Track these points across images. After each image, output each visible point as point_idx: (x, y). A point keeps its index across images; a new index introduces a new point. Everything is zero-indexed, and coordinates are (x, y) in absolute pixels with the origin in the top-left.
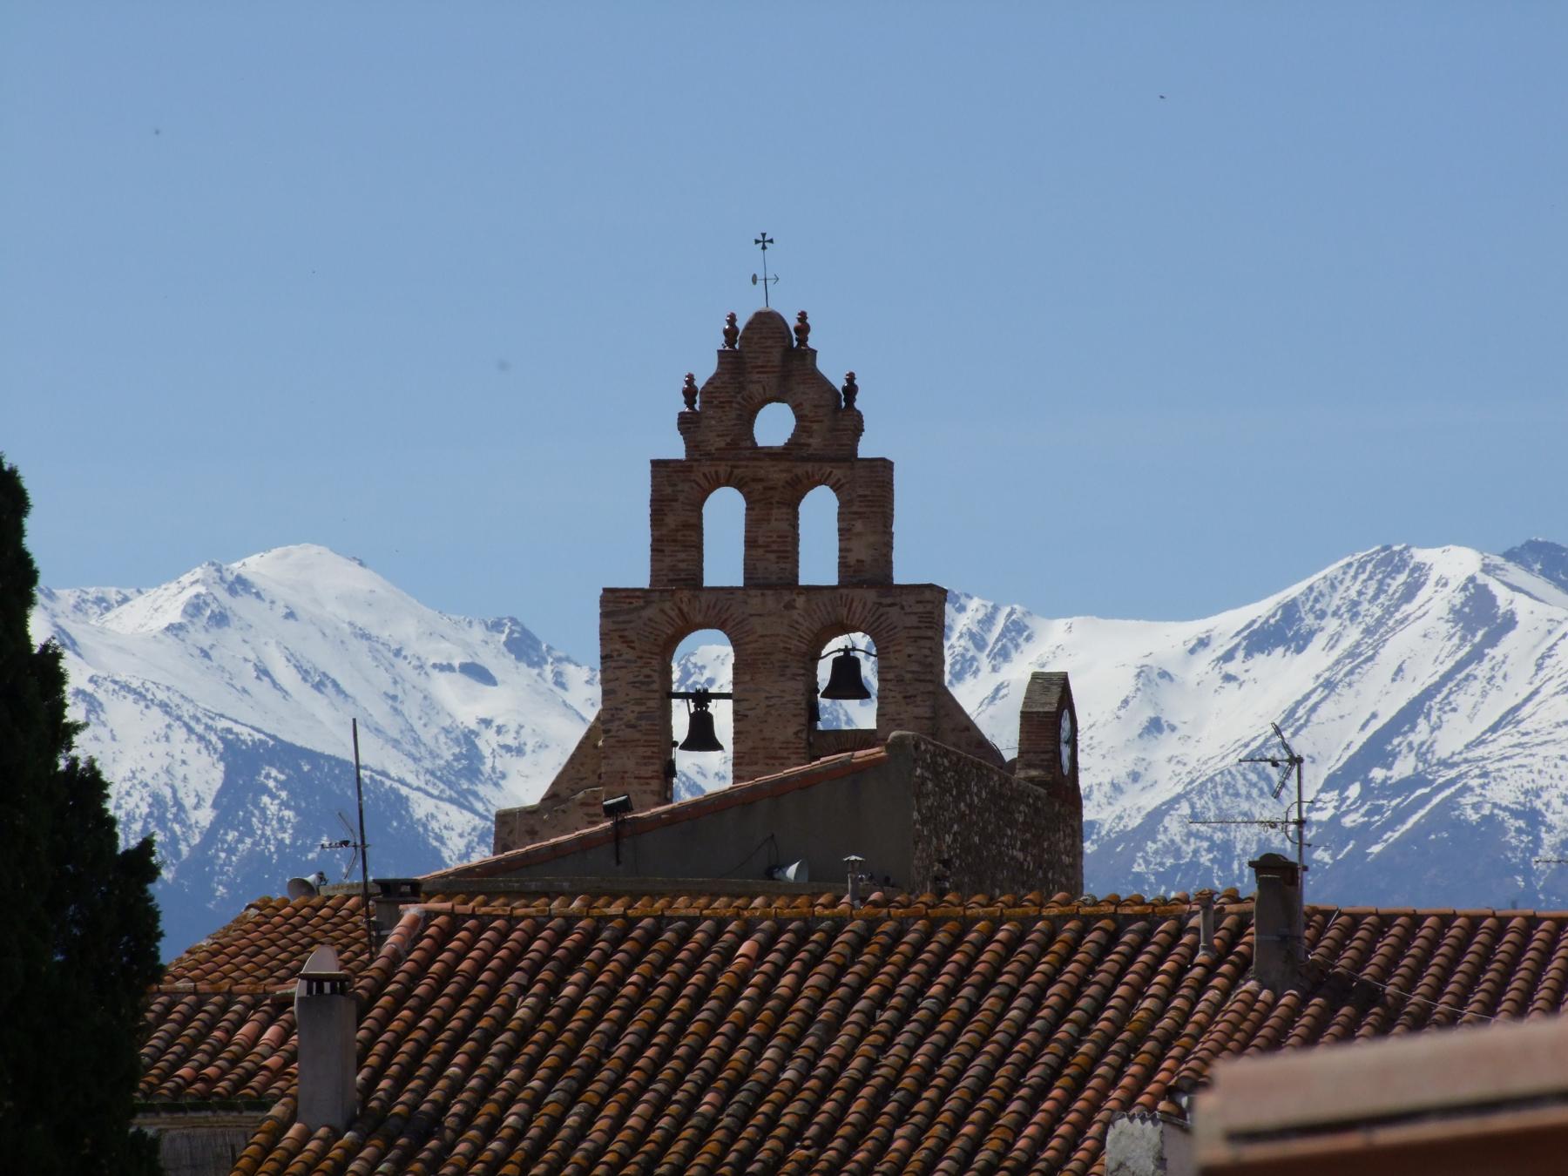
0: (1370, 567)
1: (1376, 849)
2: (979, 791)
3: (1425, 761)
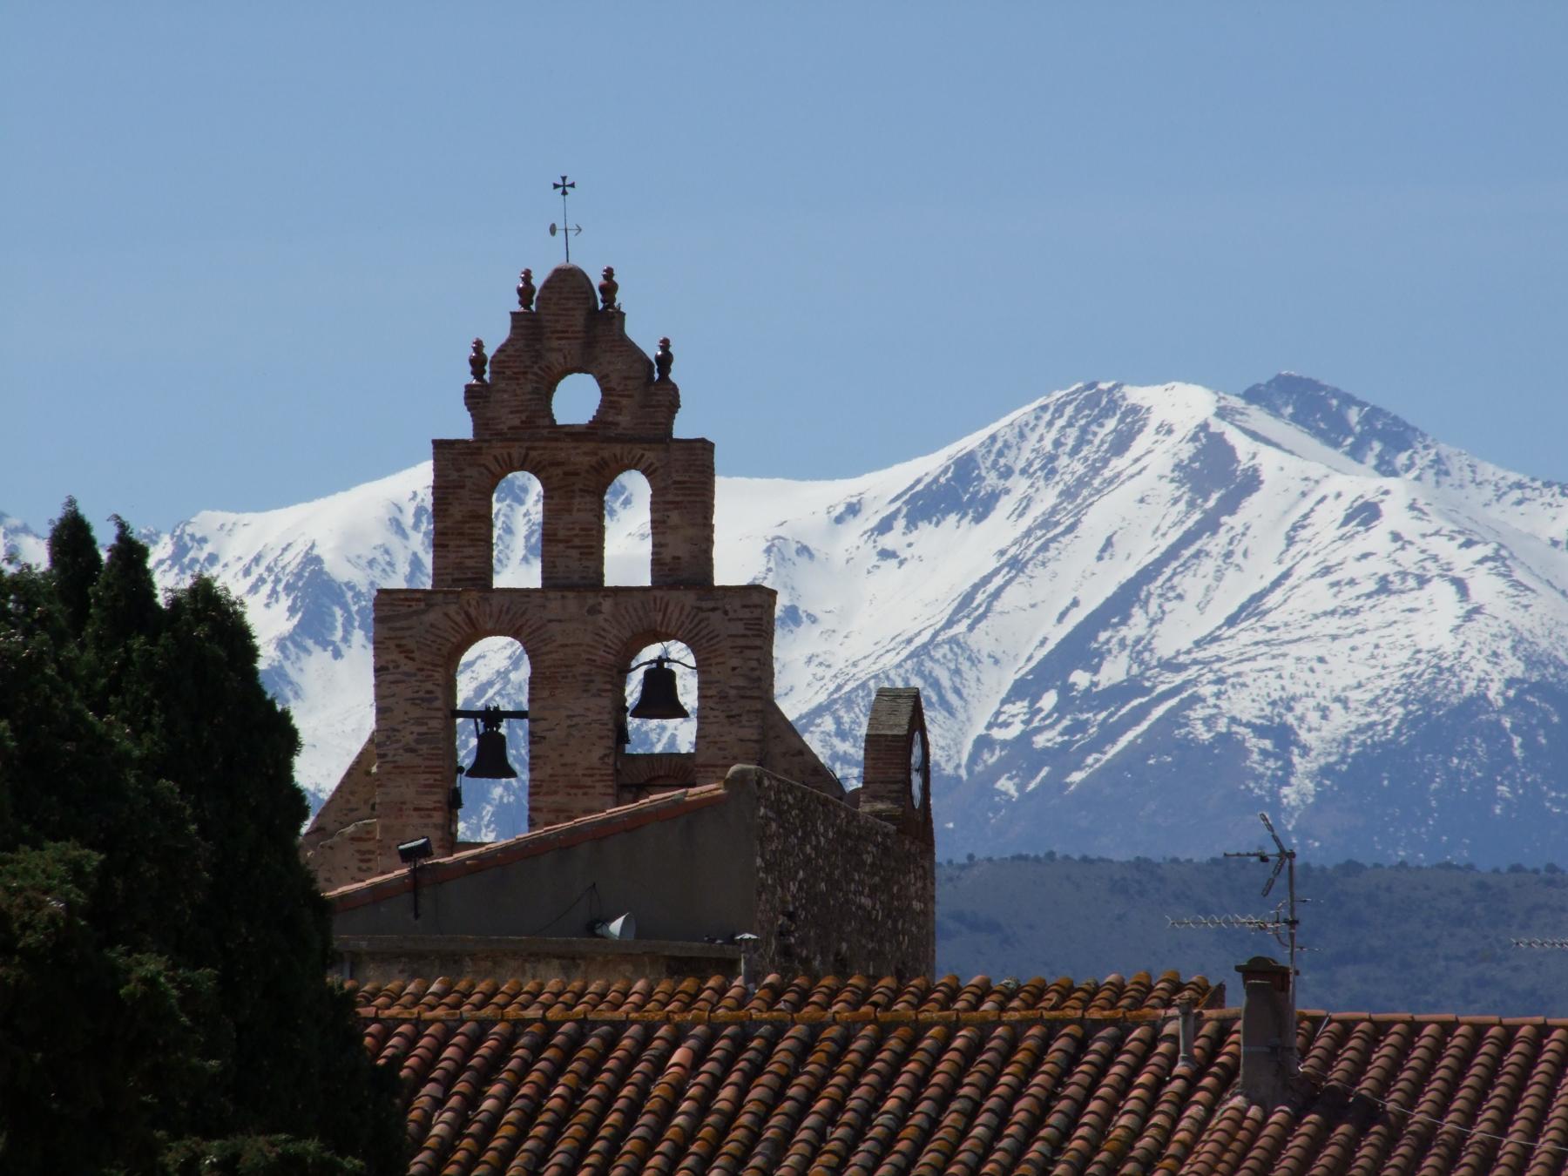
0: (1069, 410)
1: (1077, 777)
2: (826, 831)
3: (1142, 663)
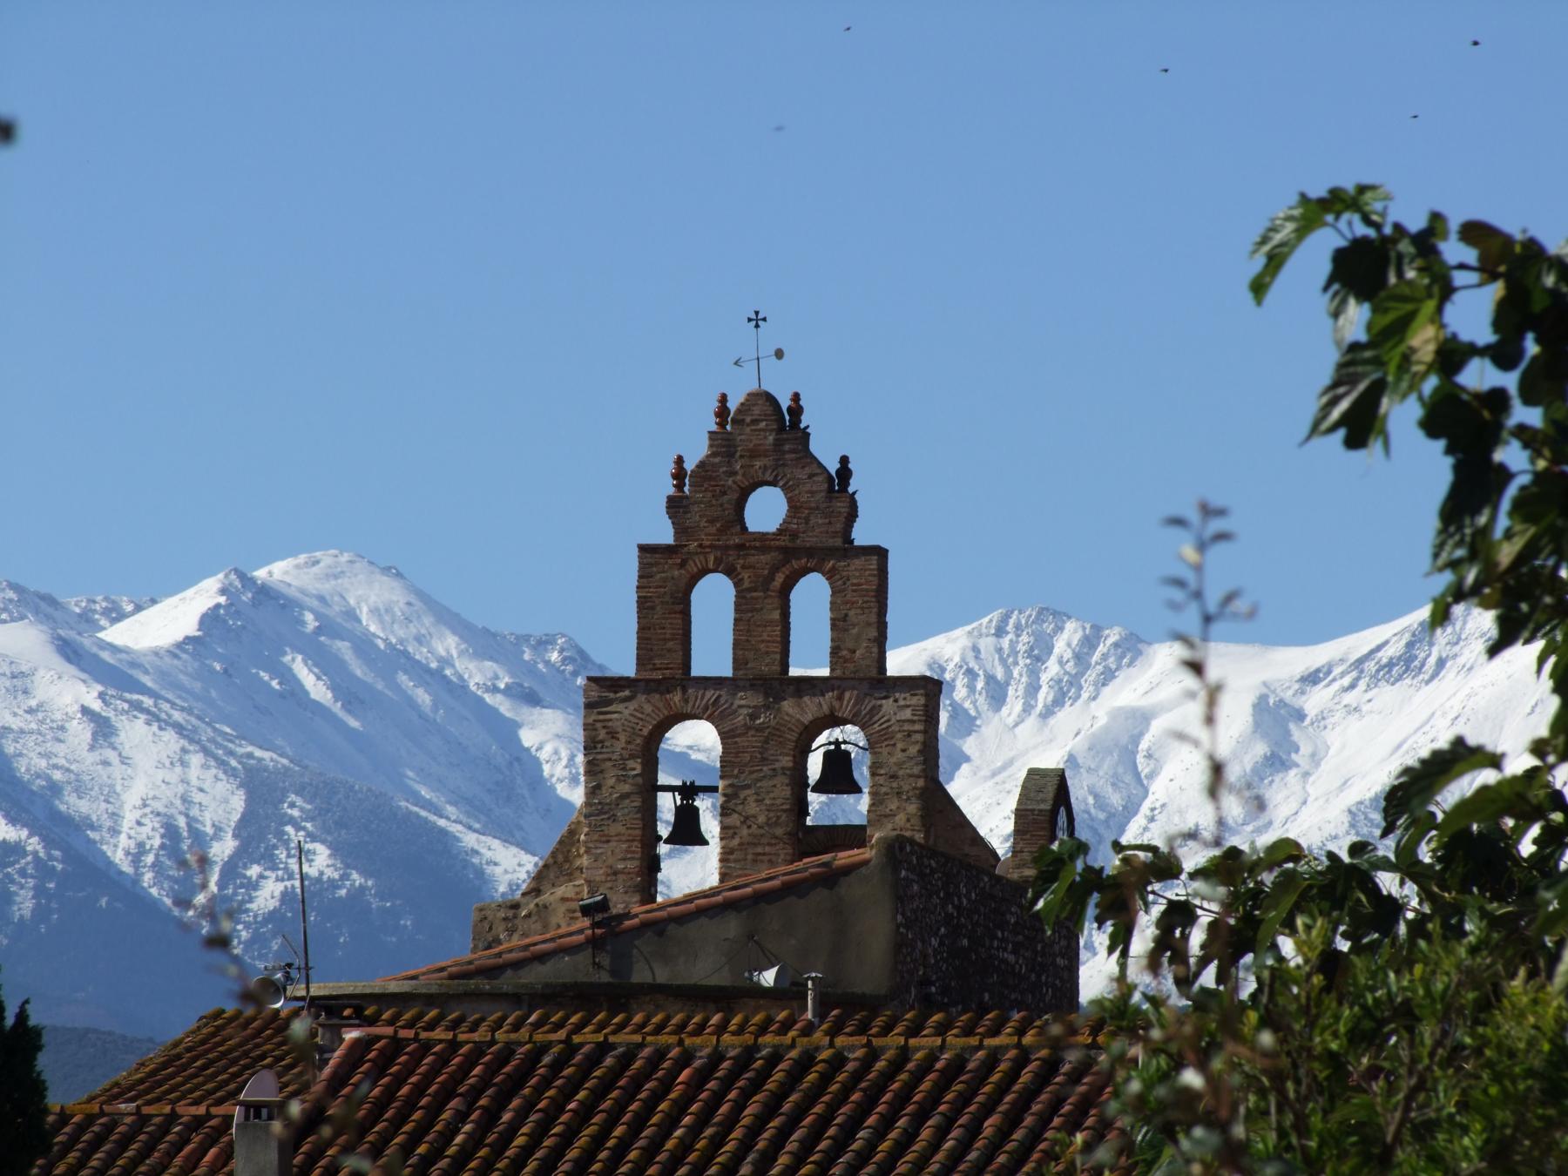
2: (969, 892)
